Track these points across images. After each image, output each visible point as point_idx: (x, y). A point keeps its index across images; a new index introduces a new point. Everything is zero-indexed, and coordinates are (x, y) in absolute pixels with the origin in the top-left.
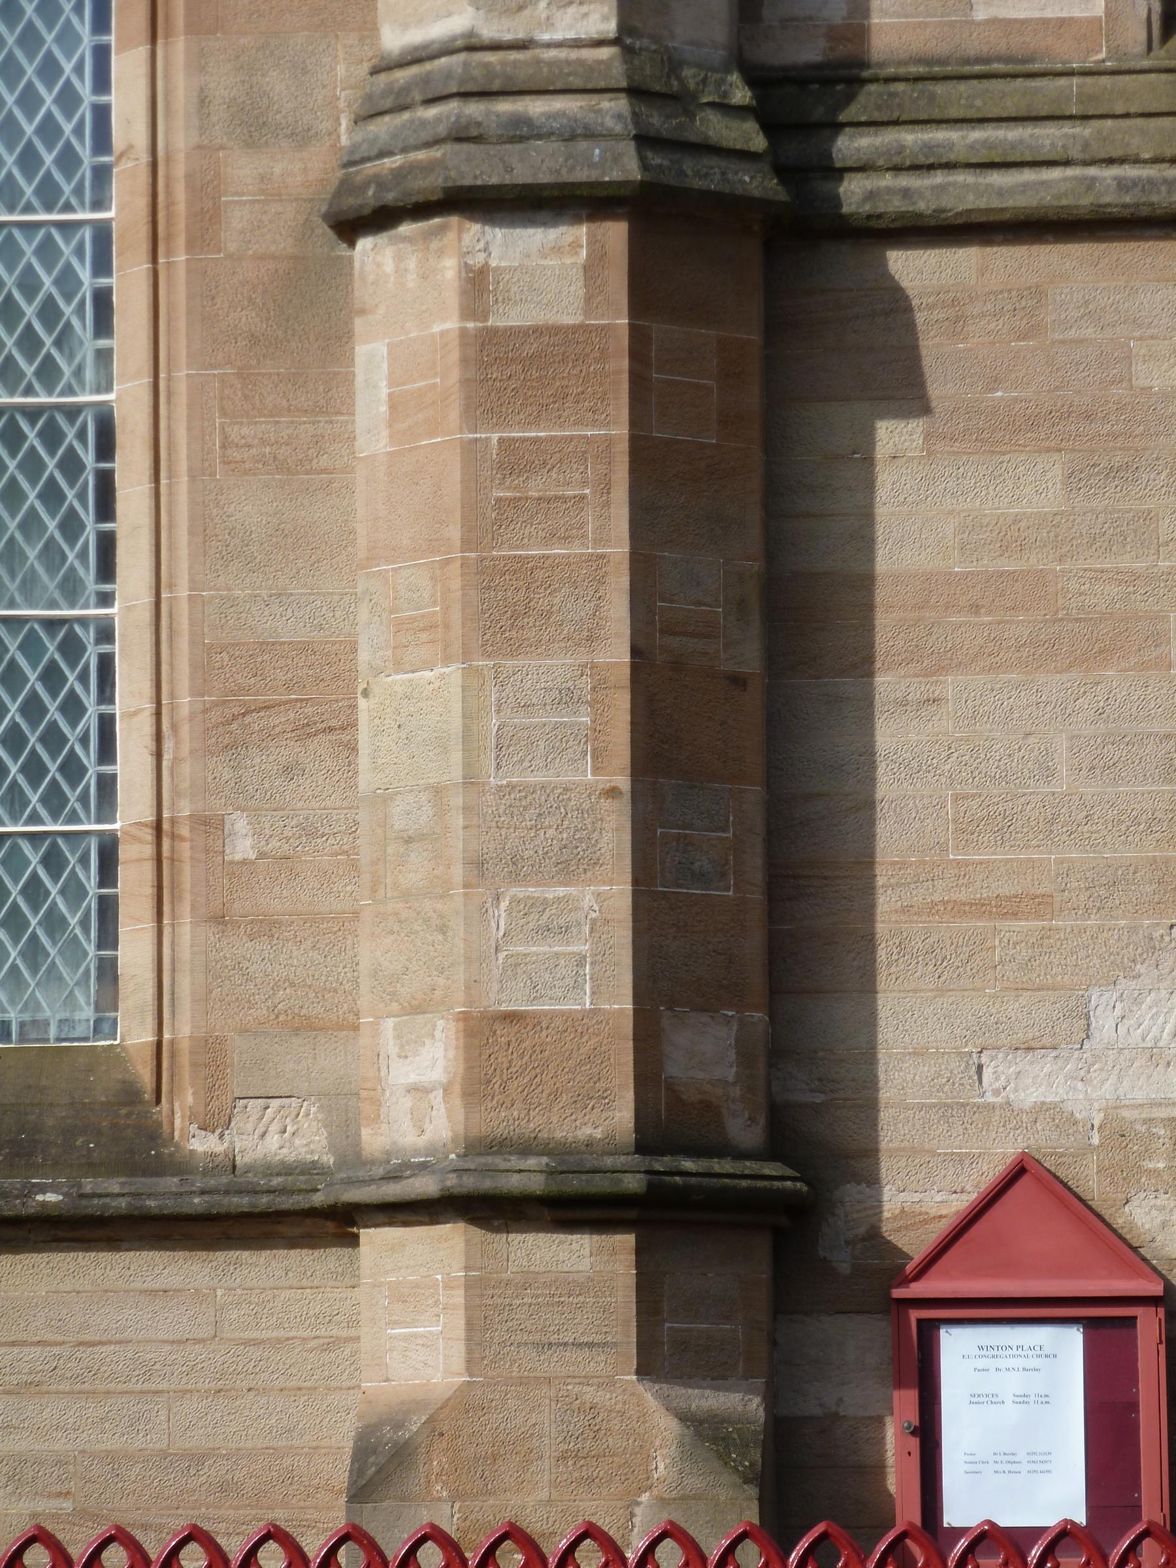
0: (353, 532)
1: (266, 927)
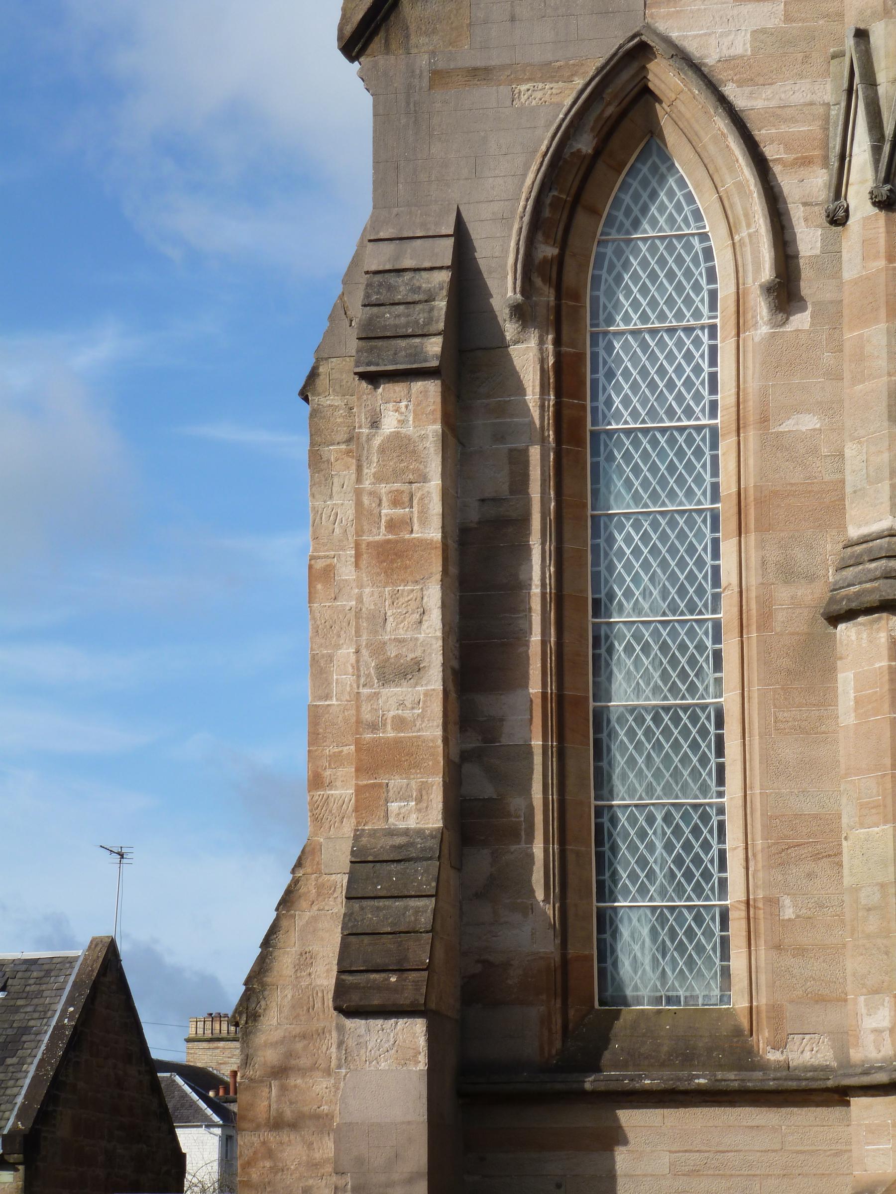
0: (838, 761)
1: (801, 951)
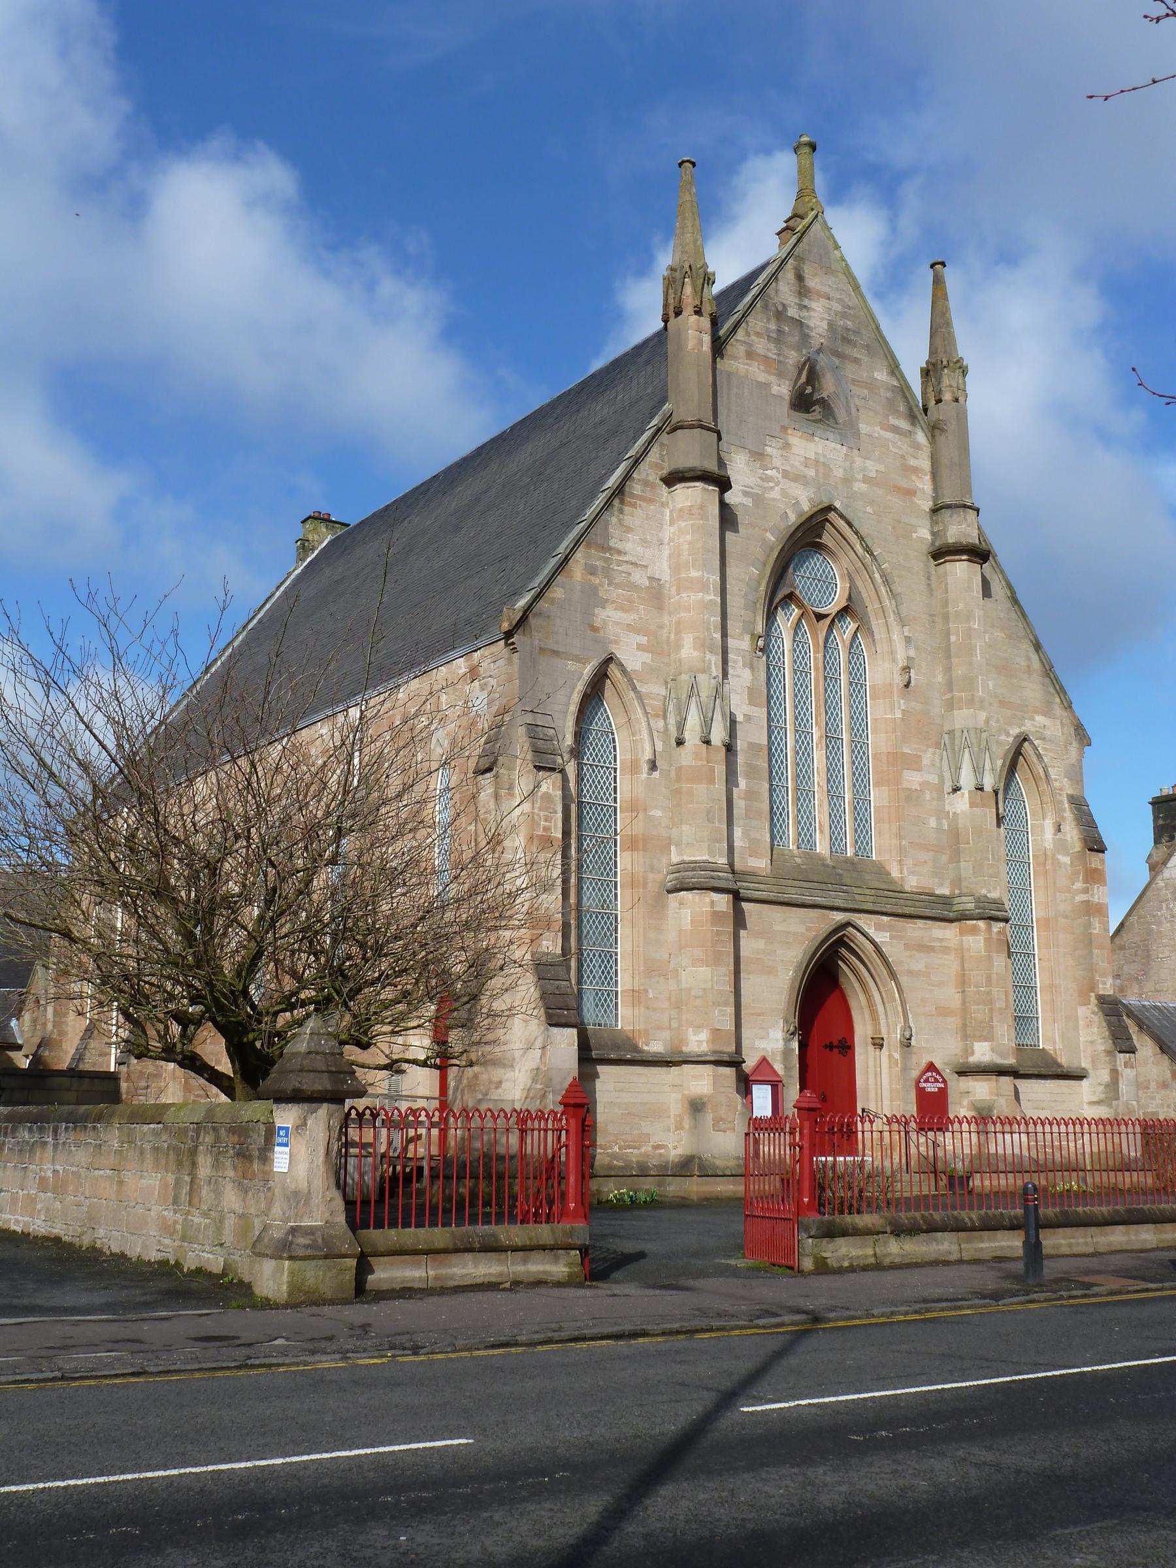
1: (655, 1010)
